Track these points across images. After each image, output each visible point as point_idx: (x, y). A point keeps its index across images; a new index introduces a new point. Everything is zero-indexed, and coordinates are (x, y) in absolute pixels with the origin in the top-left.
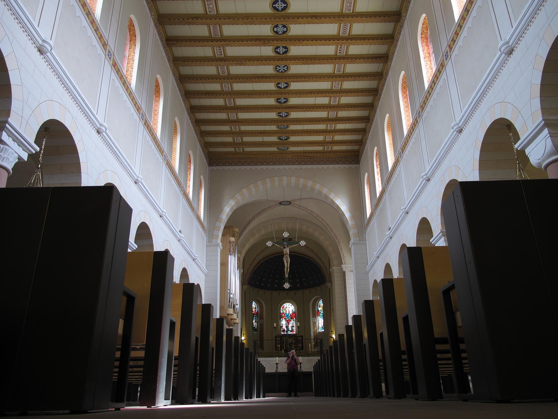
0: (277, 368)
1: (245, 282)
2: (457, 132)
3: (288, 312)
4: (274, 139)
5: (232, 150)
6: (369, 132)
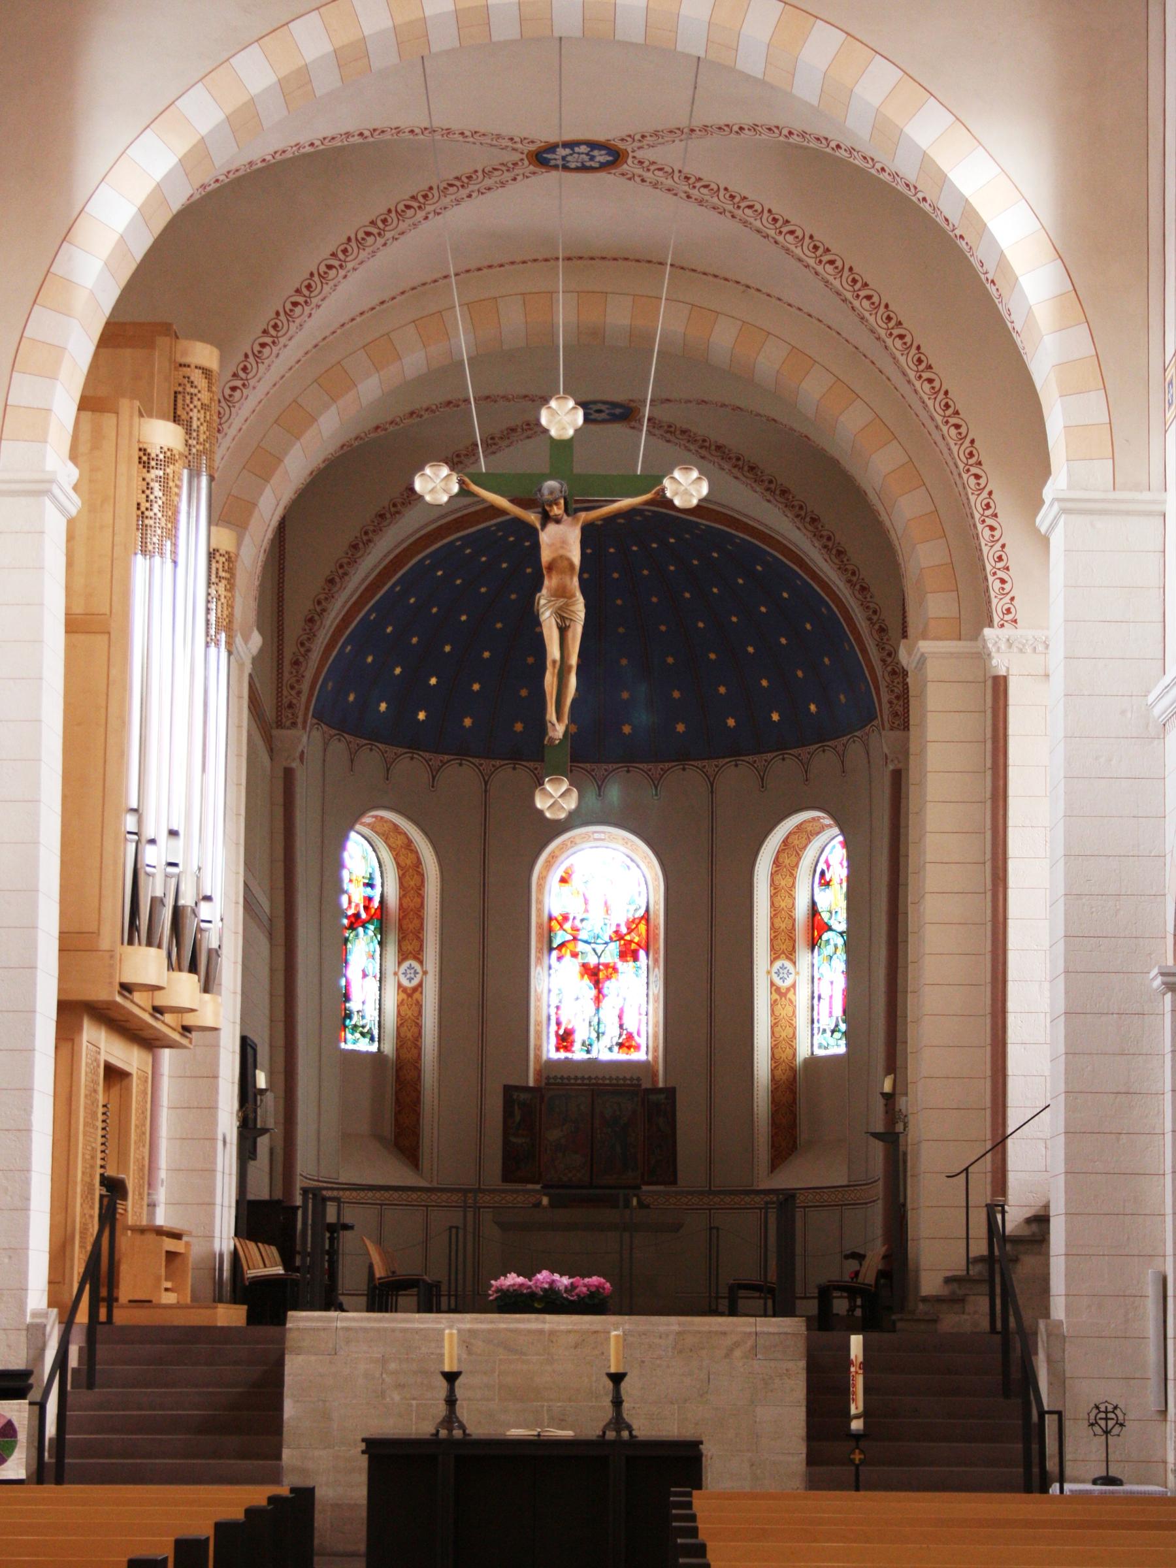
0: (451, 1401)
1: (273, 709)
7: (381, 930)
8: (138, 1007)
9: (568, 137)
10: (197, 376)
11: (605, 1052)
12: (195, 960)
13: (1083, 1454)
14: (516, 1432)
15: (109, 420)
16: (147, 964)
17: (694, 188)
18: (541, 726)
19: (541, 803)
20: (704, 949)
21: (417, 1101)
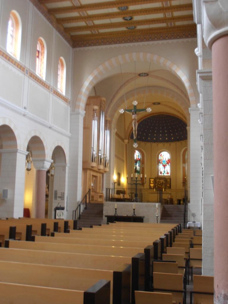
0: (116, 212)
3: (164, 159)
4: (120, 20)
5: (88, 32)
7: (140, 161)
11: (165, 175)
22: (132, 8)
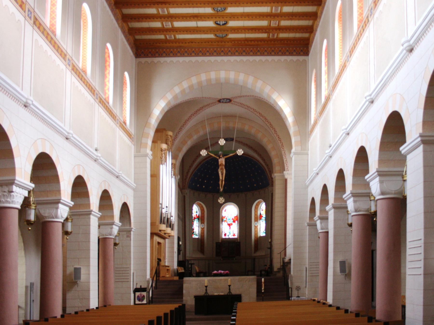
0: (206, 290)
1: (182, 187)
2: (407, 51)
4: (210, 24)
5: (162, 37)
6: (320, 17)
7: (198, 219)
8: (162, 233)
9: (223, 98)
10: (169, 137)
11: (231, 237)
12: (170, 225)
13: (295, 293)
14: (216, 294)
15: (156, 144)
16: (163, 227)
17: (241, 105)
18: (219, 189)
19: (219, 201)
20: (245, 220)
21: (204, 244)
22: (231, 10)
